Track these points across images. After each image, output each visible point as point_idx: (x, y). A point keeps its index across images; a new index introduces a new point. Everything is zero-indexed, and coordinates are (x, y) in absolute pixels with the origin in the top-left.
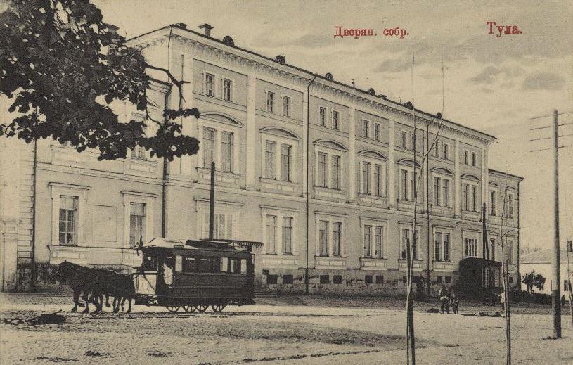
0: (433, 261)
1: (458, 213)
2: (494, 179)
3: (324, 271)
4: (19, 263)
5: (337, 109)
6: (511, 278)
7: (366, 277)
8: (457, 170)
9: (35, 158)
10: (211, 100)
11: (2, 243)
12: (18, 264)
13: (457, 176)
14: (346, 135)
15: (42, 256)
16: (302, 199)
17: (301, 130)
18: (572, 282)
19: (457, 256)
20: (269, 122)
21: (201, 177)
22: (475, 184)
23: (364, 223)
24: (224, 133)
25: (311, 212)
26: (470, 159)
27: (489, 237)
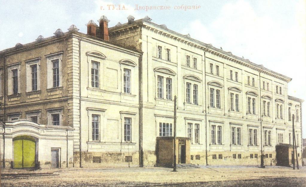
0: (210, 145)
1: (274, 120)
2: (290, 101)
3: (214, 152)
4: (74, 151)
5: (218, 64)
6: (299, 154)
7: (233, 155)
8: (245, 89)
9: (80, 94)
10: (268, 92)
11: (2, 140)
12: (74, 152)
13: (274, 100)
14: (241, 84)
15: (84, 148)
16: (203, 113)
17: (201, 77)
18: (31, 180)
19: (274, 143)
20: (188, 73)
21: (157, 103)
22: (281, 104)
23: (124, 117)
24: (167, 79)
25: (208, 121)
26: (279, 90)
27: (295, 133)
